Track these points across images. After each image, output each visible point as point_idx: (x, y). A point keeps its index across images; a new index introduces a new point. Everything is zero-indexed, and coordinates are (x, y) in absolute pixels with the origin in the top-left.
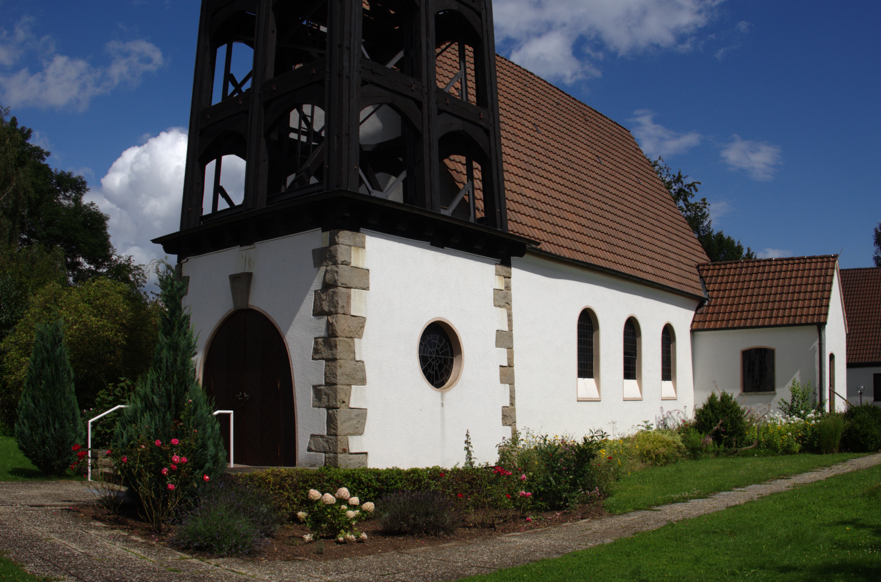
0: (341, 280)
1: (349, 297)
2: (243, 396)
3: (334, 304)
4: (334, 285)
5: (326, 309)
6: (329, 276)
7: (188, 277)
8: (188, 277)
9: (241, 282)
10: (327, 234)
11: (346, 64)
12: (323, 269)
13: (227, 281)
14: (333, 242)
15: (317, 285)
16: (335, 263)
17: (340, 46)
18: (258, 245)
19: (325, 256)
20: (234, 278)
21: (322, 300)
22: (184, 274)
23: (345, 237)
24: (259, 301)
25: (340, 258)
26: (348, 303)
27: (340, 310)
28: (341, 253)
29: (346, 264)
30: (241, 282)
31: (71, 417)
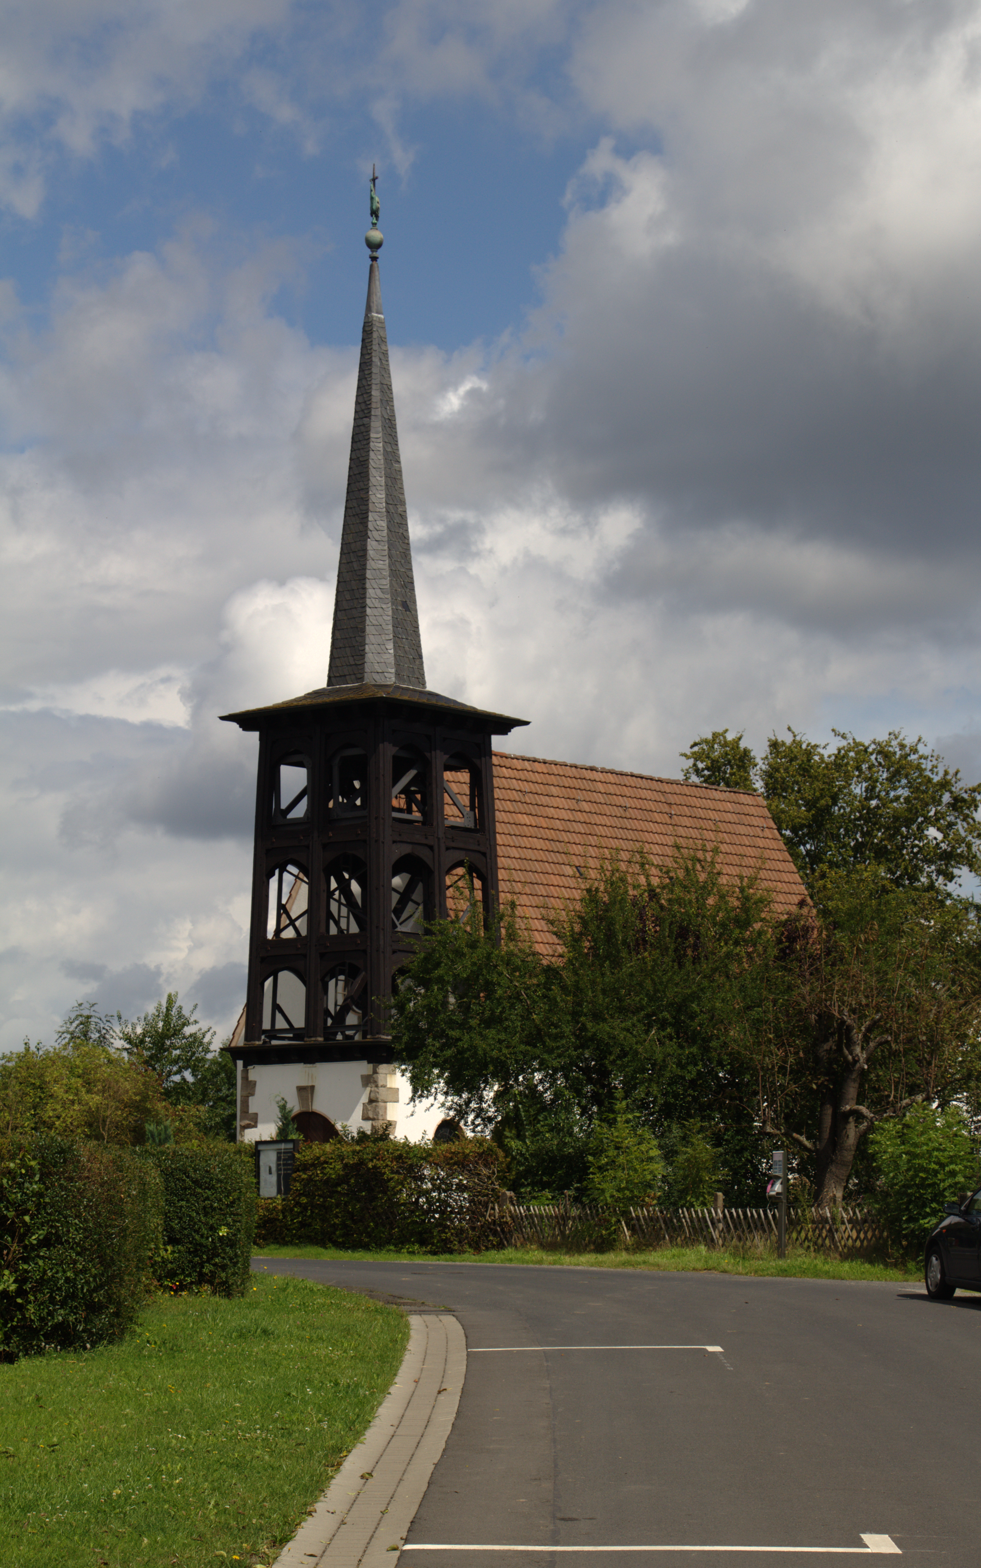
0: (380, 1098)
1: (386, 1108)
2: (541, 1081)
3: (377, 1114)
4: (376, 1101)
5: (371, 1116)
6: (373, 1095)
7: (256, 1114)
8: (256, 1114)
9: (306, 1092)
10: (371, 1065)
11: (382, 942)
12: (368, 1089)
13: (295, 1090)
14: (375, 1072)
15: (364, 1099)
16: (377, 1086)
17: (377, 927)
18: (318, 1065)
19: (369, 1080)
20: (301, 1089)
21: (367, 1110)
22: (251, 1110)
23: (383, 1068)
24: (320, 1105)
25: (380, 1083)
26: (385, 1112)
27: (380, 1118)
28: (380, 1079)
29: (384, 1086)
30: (306, 1092)
31: (270, 1201)
